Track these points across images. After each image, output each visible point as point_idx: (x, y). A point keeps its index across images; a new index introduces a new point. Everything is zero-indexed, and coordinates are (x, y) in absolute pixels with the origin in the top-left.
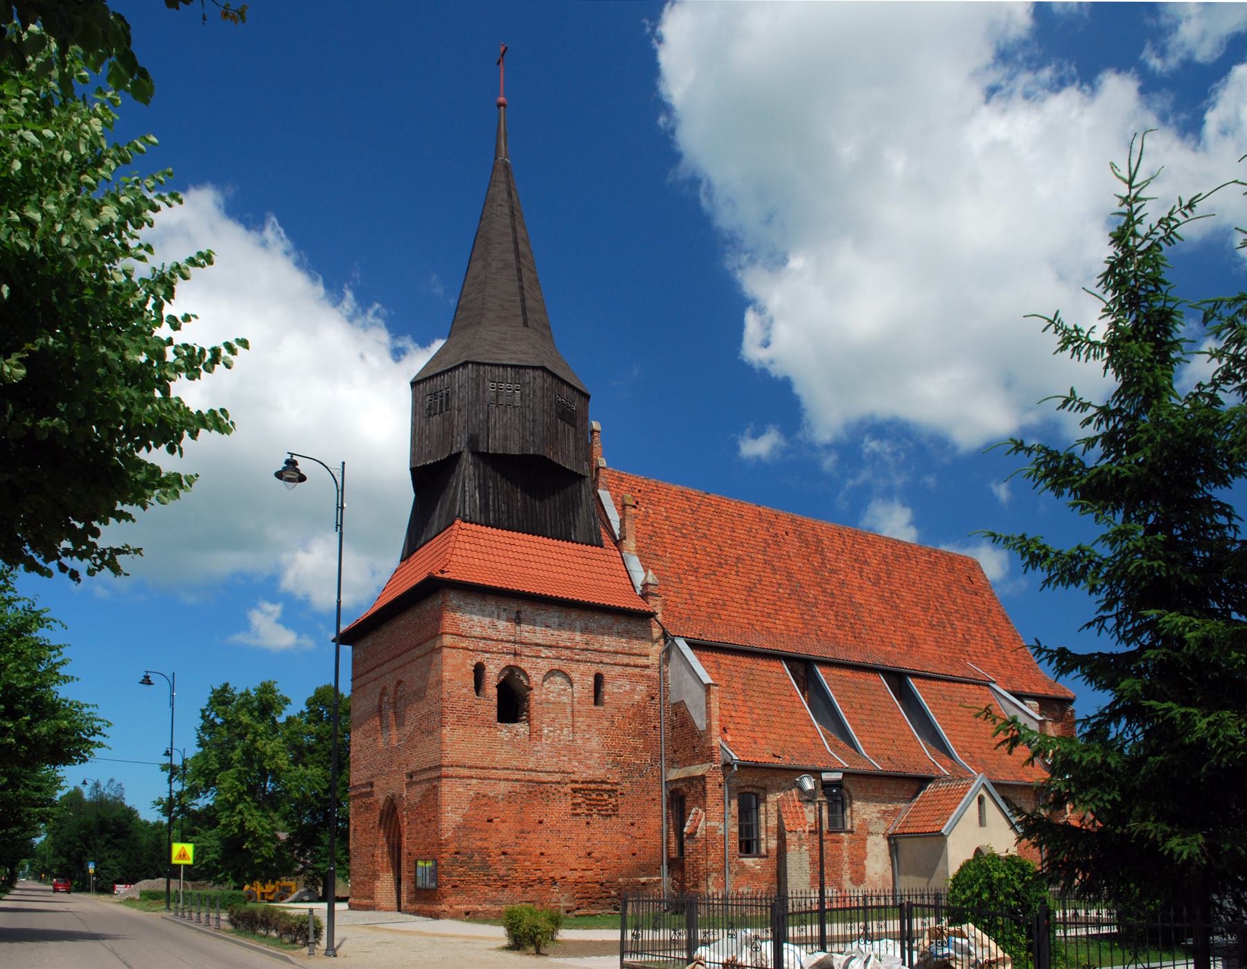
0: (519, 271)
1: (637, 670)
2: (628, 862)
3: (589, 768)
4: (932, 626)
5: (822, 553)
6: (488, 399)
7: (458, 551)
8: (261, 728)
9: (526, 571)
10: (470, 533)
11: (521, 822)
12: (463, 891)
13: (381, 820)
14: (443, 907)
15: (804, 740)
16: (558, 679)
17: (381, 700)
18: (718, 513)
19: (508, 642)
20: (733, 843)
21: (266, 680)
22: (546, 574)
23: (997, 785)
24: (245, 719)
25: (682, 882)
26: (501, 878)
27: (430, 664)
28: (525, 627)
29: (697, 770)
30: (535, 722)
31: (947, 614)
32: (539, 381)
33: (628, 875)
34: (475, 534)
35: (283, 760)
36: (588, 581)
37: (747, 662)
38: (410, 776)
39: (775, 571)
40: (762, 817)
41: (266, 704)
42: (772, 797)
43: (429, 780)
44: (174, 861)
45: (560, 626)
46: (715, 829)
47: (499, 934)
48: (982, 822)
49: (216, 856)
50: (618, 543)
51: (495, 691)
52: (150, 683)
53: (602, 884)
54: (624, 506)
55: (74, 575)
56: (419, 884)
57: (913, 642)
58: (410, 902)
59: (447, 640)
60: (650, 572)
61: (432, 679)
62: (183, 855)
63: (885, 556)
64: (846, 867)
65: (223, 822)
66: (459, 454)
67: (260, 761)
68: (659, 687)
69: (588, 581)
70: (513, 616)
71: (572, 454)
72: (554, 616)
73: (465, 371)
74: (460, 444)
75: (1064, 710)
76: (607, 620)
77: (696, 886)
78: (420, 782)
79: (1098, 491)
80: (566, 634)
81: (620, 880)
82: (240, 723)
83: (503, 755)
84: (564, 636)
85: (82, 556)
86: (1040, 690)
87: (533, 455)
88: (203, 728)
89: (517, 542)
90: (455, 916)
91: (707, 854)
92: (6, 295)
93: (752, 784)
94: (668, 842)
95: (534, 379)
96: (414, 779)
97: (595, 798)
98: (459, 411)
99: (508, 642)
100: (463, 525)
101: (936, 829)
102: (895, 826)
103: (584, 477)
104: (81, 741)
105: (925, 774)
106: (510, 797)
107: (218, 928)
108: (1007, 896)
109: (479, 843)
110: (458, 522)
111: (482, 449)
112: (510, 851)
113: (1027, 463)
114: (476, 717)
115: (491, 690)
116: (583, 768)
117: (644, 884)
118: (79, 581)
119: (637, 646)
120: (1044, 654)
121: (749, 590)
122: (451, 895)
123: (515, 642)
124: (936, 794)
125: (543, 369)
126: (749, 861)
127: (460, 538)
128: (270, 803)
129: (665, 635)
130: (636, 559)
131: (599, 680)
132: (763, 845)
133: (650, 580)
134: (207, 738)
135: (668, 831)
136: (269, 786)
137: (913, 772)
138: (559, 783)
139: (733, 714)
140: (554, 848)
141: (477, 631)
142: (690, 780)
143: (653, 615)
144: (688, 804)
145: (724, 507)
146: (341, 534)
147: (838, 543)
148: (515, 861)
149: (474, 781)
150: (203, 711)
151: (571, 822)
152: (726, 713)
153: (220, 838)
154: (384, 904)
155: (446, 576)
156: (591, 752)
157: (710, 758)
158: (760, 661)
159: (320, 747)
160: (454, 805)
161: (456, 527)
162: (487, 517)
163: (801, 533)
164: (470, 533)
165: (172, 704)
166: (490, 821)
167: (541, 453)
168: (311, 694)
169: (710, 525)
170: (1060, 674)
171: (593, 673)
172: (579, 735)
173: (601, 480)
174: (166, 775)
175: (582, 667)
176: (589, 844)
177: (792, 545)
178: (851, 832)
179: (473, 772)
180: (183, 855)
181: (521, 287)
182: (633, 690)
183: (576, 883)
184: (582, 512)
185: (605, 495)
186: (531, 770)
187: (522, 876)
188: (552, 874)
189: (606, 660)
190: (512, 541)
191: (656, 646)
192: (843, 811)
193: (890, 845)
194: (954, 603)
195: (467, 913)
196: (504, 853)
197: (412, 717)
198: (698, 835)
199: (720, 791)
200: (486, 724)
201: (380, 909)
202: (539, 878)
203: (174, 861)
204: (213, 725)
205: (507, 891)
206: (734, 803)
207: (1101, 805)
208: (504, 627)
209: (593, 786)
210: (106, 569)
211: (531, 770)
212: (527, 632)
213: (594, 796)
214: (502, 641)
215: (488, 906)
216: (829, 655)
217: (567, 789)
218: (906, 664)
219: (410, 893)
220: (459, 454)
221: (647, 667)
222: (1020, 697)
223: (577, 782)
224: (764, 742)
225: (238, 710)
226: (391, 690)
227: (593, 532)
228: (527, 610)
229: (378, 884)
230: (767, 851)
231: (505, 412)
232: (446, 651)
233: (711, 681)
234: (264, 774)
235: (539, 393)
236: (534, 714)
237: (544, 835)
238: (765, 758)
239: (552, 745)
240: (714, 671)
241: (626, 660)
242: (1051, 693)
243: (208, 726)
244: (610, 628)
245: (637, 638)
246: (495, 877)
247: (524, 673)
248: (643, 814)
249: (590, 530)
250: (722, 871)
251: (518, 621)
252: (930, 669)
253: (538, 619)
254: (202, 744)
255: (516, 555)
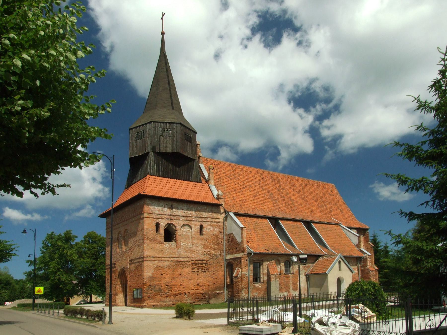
0: (170, 91)
1: (215, 223)
2: (213, 286)
3: (198, 256)
4: (319, 206)
5: (280, 183)
6: (159, 134)
7: (149, 185)
8: (66, 246)
9: (174, 191)
10: (153, 179)
11: (173, 274)
12: (152, 299)
13: (119, 276)
14: (145, 304)
15: (276, 244)
16: (187, 227)
17: (118, 235)
18: (242, 171)
19: (168, 215)
20: (251, 279)
21: (90, 231)
22: (182, 192)
23: (344, 257)
24: (60, 243)
25: (233, 292)
26: (166, 294)
27: (139, 223)
28: (174, 210)
29: (238, 255)
30: (178, 242)
31: (324, 202)
32: (179, 128)
33: (213, 291)
34: (155, 180)
35: (75, 257)
36: (197, 195)
37: (255, 220)
38: (131, 261)
39: (263, 189)
40: (262, 270)
41: (68, 238)
42: (265, 264)
43: (139, 262)
44: (36, 293)
45: (187, 210)
46: (245, 275)
47: (173, 312)
48: (340, 269)
49: (49, 290)
50: (207, 182)
51: (164, 232)
52: (26, 233)
53: (203, 294)
54: (209, 169)
55: (36, 195)
56: (135, 297)
57: (312, 212)
58: (131, 303)
59: (146, 215)
60: (220, 191)
61: (140, 228)
62: (39, 291)
63: (302, 184)
64: (291, 285)
65: (52, 278)
66: (148, 153)
67: (65, 257)
68: (223, 229)
69: (197, 195)
70: (170, 206)
71: (191, 152)
72: (185, 206)
73: (151, 125)
74: (149, 149)
75: (365, 232)
76: (204, 207)
77: (238, 293)
78: (135, 263)
79: (424, 159)
80: (189, 212)
81: (209, 292)
82: (58, 245)
83: (166, 253)
84: (189, 213)
85: (41, 188)
86: (357, 226)
87: (177, 153)
88: (43, 247)
89: (170, 182)
90: (149, 307)
91: (242, 283)
92: (39, 85)
93: (257, 259)
94: (226, 279)
95: (177, 127)
96: (133, 262)
97: (200, 266)
98: (148, 138)
99: (168, 215)
100: (150, 176)
101: (324, 272)
102: (308, 271)
103: (195, 160)
104: (7, 253)
105: (317, 254)
106: (169, 267)
107: (58, 316)
108: (369, 294)
109: (158, 282)
110: (148, 175)
111: (157, 151)
112: (169, 284)
113: (400, 150)
114: (157, 240)
115: (162, 231)
116: (196, 256)
117: (218, 293)
118: (38, 197)
119: (215, 215)
120: (404, 214)
121: (254, 196)
122: (147, 300)
123: (171, 215)
124: (323, 261)
125: (180, 123)
126: (257, 285)
127: (149, 181)
128: (69, 271)
129: (225, 212)
130: (214, 187)
131: (201, 227)
132: (262, 279)
133: (220, 193)
134: (45, 251)
135: (227, 276)
136: (70, 266)
137: (315, 254)
138: (187, 261)
139: (251, 237)
140: (186, 283)
141: (157, 212)
142: (235, 259)
143: (221, 205)
144: (234, 267)
145: (244, 169)
146: (113, 180)
147: (285, 180)
148: (171, 288)
149: (156, 262)
150: (43, 241)
151: (191, 274)
152: (248, 236)
153: (50, 284)
154: (120, 304)
155: (145, 193)
156: (199, 251)
157: (243, 251)
158: (259, 219)
159: (89, 252)
160: (148, 270)
161: (148, 177)
162: (159, 174)
163: (272, 177)
164: (153, 179)
165: (35, 240)
166: (162, 275)
167: (179, 152)
168: (86, 234)
169: (240, 175)
170: (410, 221)
171: (199, 225)
172: (194, 246)
173: (200, 161)
174: (28, 264)
175: (195, 223)
176: (198, 281)
177: (269, 181)
178: (293, 274)
179: (156, 259)
180: (39, 291)
181: (171, 96)
182: (214, 230)
183: (193, 294)
184: (194, 172)
185: (202, 166)
186: (177, 257)
187: (174, 293)
188: (185, 292)
189: (204, 220)
190: (169, 182)
191: (222, 215)
192: (290, 267)
193: (306, 277)
194: (326, 198)
195: (154, 306)
196: (167, 285)
197: (131, 242)
198: (239, 277)
199: (247, 262)
200: (160, 242)
201: (118, 306)
202: (180, 293)
203: (36, 293)
204: (47, 246)
205: (168, 298)
206: (252, 266)
207: (435, 263)
208: (166, 210)
209: (199, 262)
210: (50, 193)
211: (177, 257)
212: (175, 212)
213: (200, 265)
214: (166, 215)
215: (161, 303)
216: (284, 217)
217: (190, 263)
218: (310, 219)
219: (131, 299)
220: (148, 153)
221: (219, 222)
222: (351, 228)
223: (193, 261)
224: (262, 245)
225: (56, 241)
226: (122, 233)
227: (199, 178)
228: (175, 204)
229: (117, 297)
230: (263, 281)
231: (166, 138)
232: (145, 219)
233: (243, 226)
234: (67, 262)
235: (179, 132)
236: (178, 239)
237: (182, 278)
238: (263, 251)
239: (184, 249)
240: (243, 223)
241: (211, 220)
242: (361, 227)
243: (45, 246)
244: (205, 210)
245: (215, 213)
246: (164, 293)
247: (174, 225)
248: (218, 271)
249: (197, 177)
250: (248, 288)
251: (172, 208)
252: (319, 220)
253: (179, 207)
254: (42, 252)
255: (170, 186)
